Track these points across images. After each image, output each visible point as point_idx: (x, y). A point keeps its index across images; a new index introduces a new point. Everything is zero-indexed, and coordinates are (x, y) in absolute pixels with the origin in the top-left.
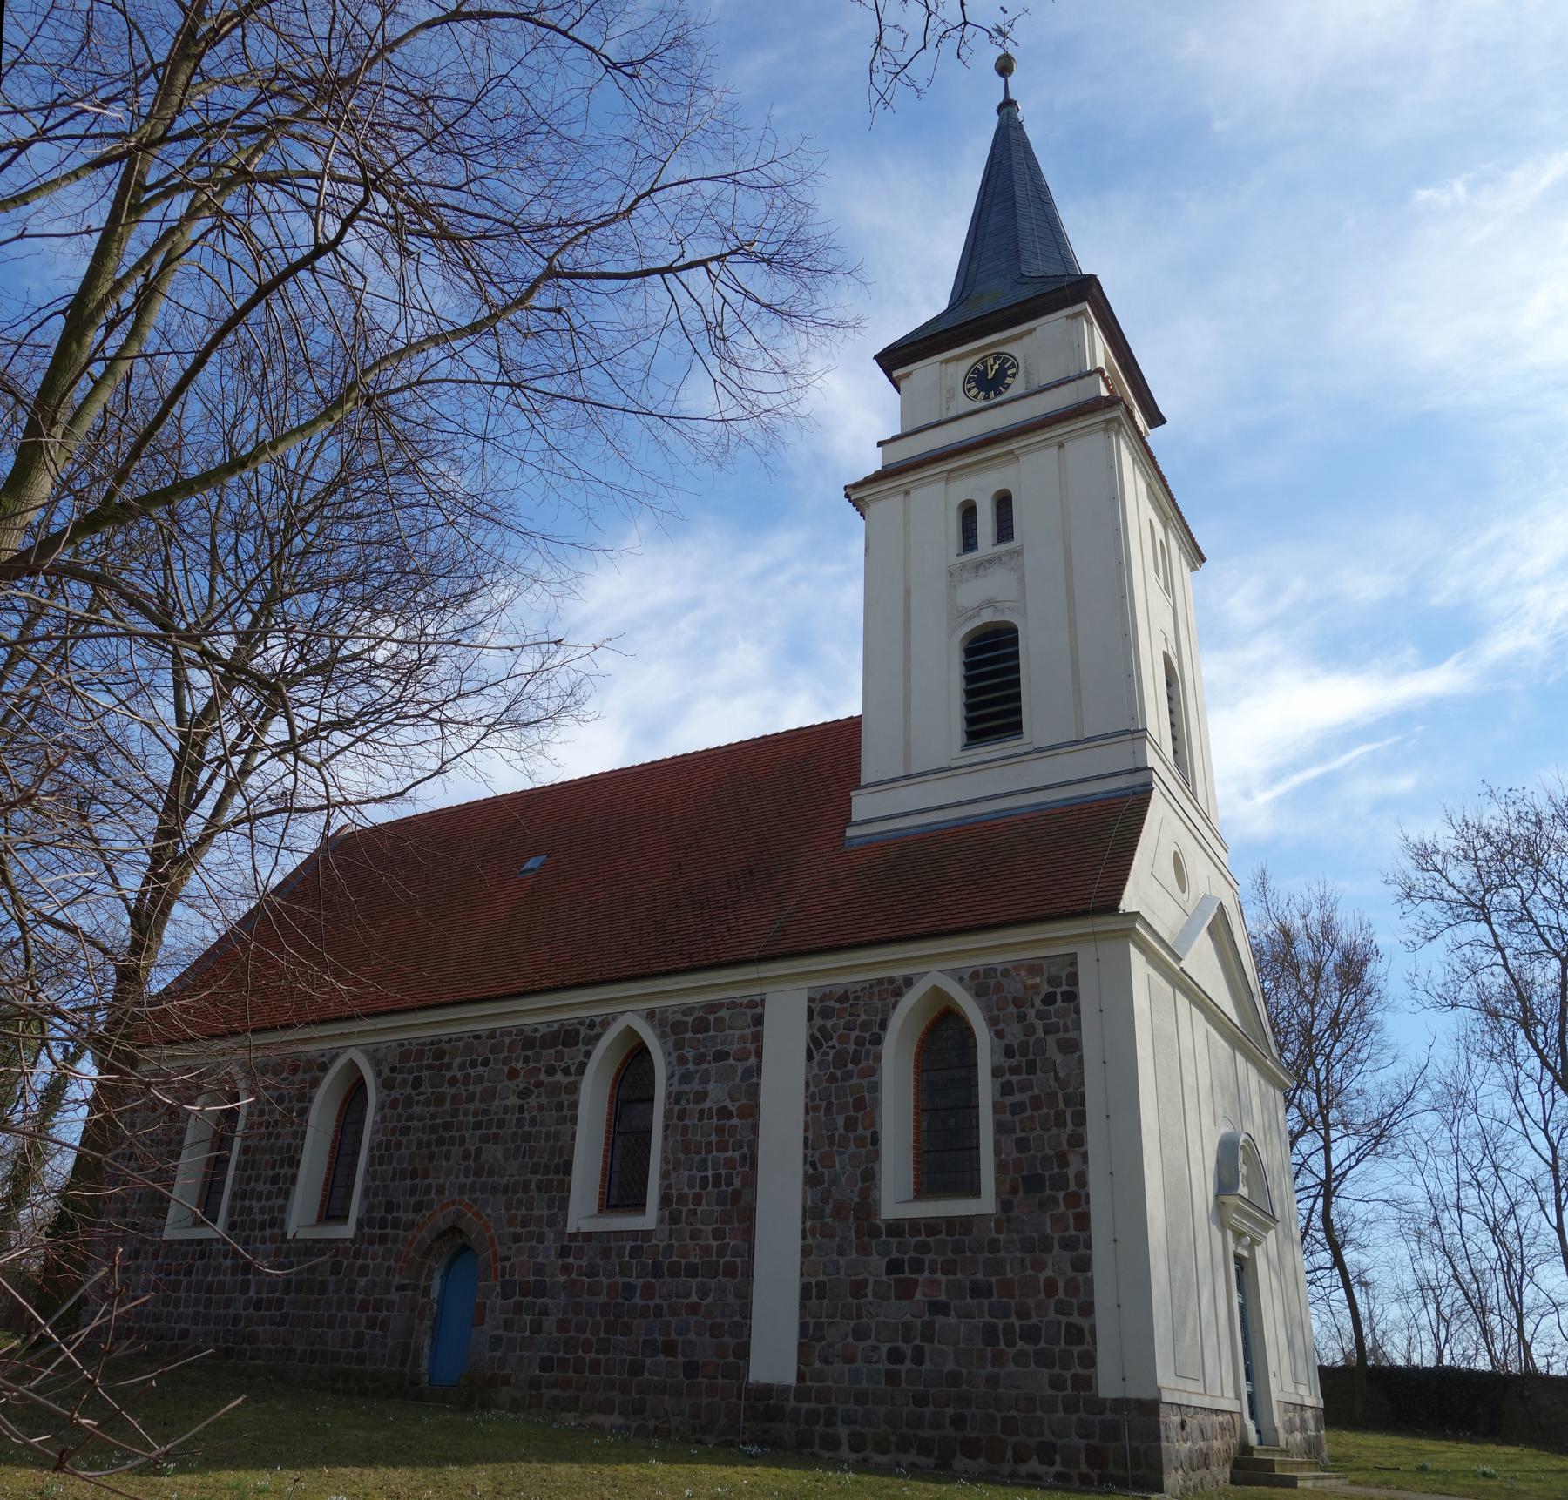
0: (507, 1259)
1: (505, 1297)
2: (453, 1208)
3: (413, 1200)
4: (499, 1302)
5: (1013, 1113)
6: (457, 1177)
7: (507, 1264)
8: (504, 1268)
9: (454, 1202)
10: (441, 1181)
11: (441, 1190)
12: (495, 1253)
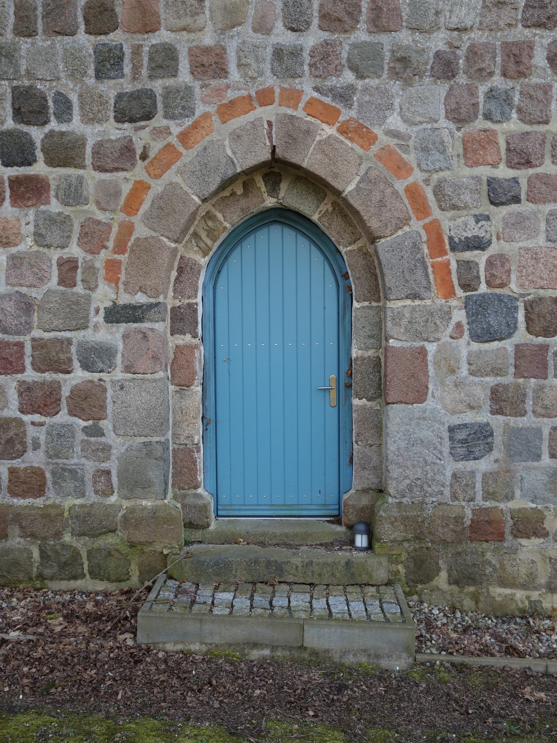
0: (479, 244)
1: (484, 335)
2: (266, 113)
3: (110, 89)
4: (465, 347)
5: (271, 91)
6: (263, 27)
7: (481, 258)
8: (467, 266)
9: (265, 97)
10: (208, 39)
11: (211, 64)
12: (434, 229)
